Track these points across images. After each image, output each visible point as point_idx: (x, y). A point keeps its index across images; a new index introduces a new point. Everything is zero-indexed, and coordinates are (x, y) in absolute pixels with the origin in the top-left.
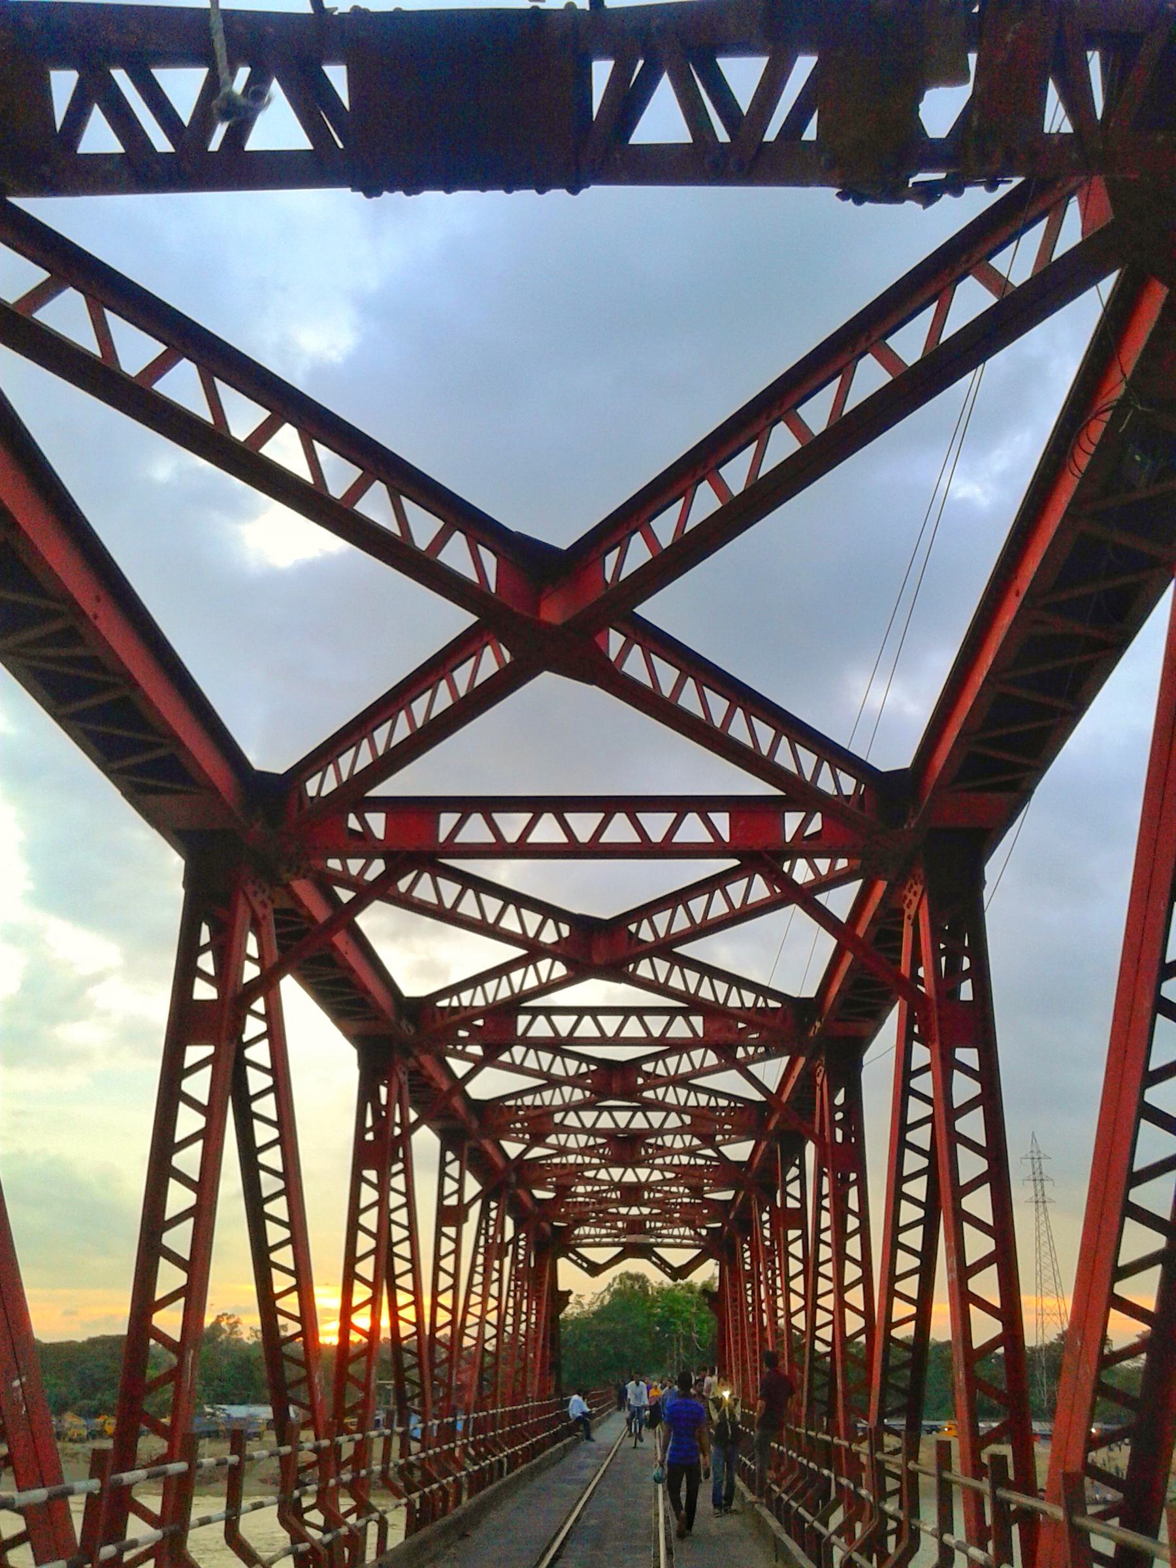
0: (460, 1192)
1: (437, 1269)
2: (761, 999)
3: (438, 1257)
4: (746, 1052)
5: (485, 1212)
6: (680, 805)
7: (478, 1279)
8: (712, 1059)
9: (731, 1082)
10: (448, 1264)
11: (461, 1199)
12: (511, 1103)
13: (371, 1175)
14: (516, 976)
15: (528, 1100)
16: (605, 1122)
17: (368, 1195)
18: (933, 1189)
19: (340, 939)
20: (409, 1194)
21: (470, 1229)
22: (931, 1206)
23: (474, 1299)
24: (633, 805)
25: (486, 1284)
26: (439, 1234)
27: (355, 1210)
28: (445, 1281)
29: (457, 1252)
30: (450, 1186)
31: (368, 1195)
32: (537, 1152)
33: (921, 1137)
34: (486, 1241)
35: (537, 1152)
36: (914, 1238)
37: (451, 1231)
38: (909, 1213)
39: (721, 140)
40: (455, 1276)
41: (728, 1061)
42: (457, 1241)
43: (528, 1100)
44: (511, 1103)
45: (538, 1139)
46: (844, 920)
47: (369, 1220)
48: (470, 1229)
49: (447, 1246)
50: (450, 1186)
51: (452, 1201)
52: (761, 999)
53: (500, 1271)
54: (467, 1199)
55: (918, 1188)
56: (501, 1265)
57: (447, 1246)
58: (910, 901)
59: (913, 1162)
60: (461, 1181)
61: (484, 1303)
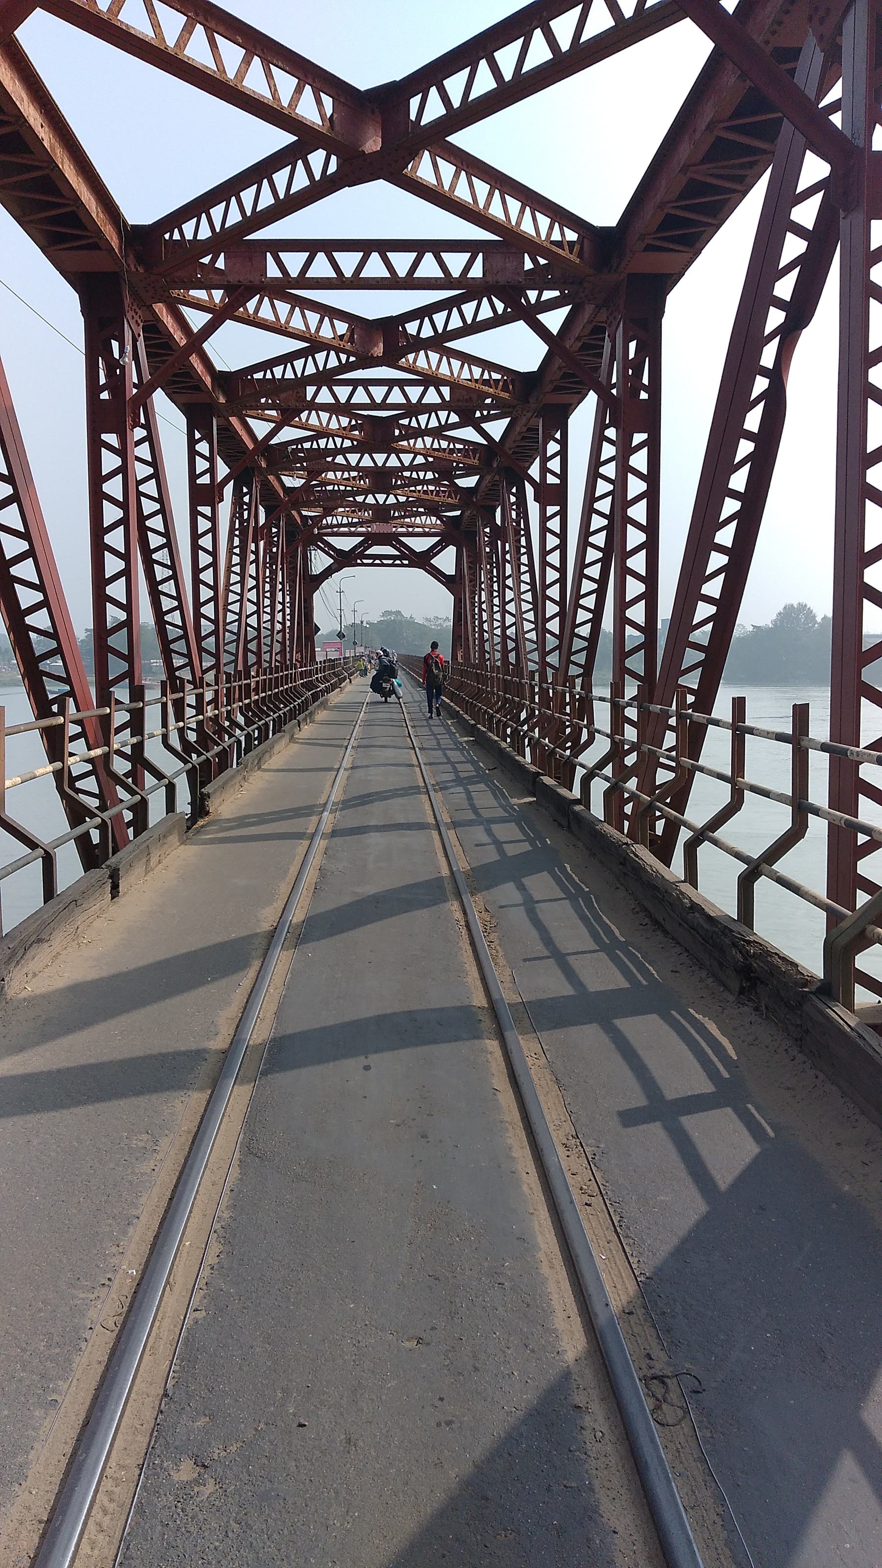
0: (212, 470)
1: (196, 548)
2: (452, 444)
3: (195, 536)
4: (482, 414)
5: (238, 495)
6: (419, 247)
7: (236, 559)
8: (454, 418)
9: (469, 434)
10: (206, 542)
11: (213, 478)
12: (259, 376)
13: (111, 438)
14: (299, 364)
15: (307, 445)
16: (367, 462)
17: (110, 461)
18: (609, 540)
19: (194, 360)
20: (155, 463)
21: (225, 509)
22: (607, 551)
23: (234, 578)
24: (384, 247)
25: (243, 565)
26: (194, 514)
27: (97, 478)
28: (204, 559)
29: (213, 530)
30: (202, 465)
31: (110, 461)
32: (288, 434)
33: (604, 506)
34: (240, 524)
35: (288, 434)
36: (594, 571)
37: (206, 510)
38: (592, 555)
39: (411, 118)
40: (214, 554)
41: (467, 420)
42: (213, 519)
43: (307, 445)
44: (259, 376)
45: (287, 418)
46: (555, 333)
47: (114, 487)
48: (225, 509)
49: (203, 525)
50: (202, 465)
51: (205, 480)
52: (452, 444)
53: (256, 553)
54: (220, 477)
55: (599, 539)
56: (257, 547)
57: (203, 525)
58: (611, 322)
59: (597, 522)
60: (211, 460)
61: (242, 582)
